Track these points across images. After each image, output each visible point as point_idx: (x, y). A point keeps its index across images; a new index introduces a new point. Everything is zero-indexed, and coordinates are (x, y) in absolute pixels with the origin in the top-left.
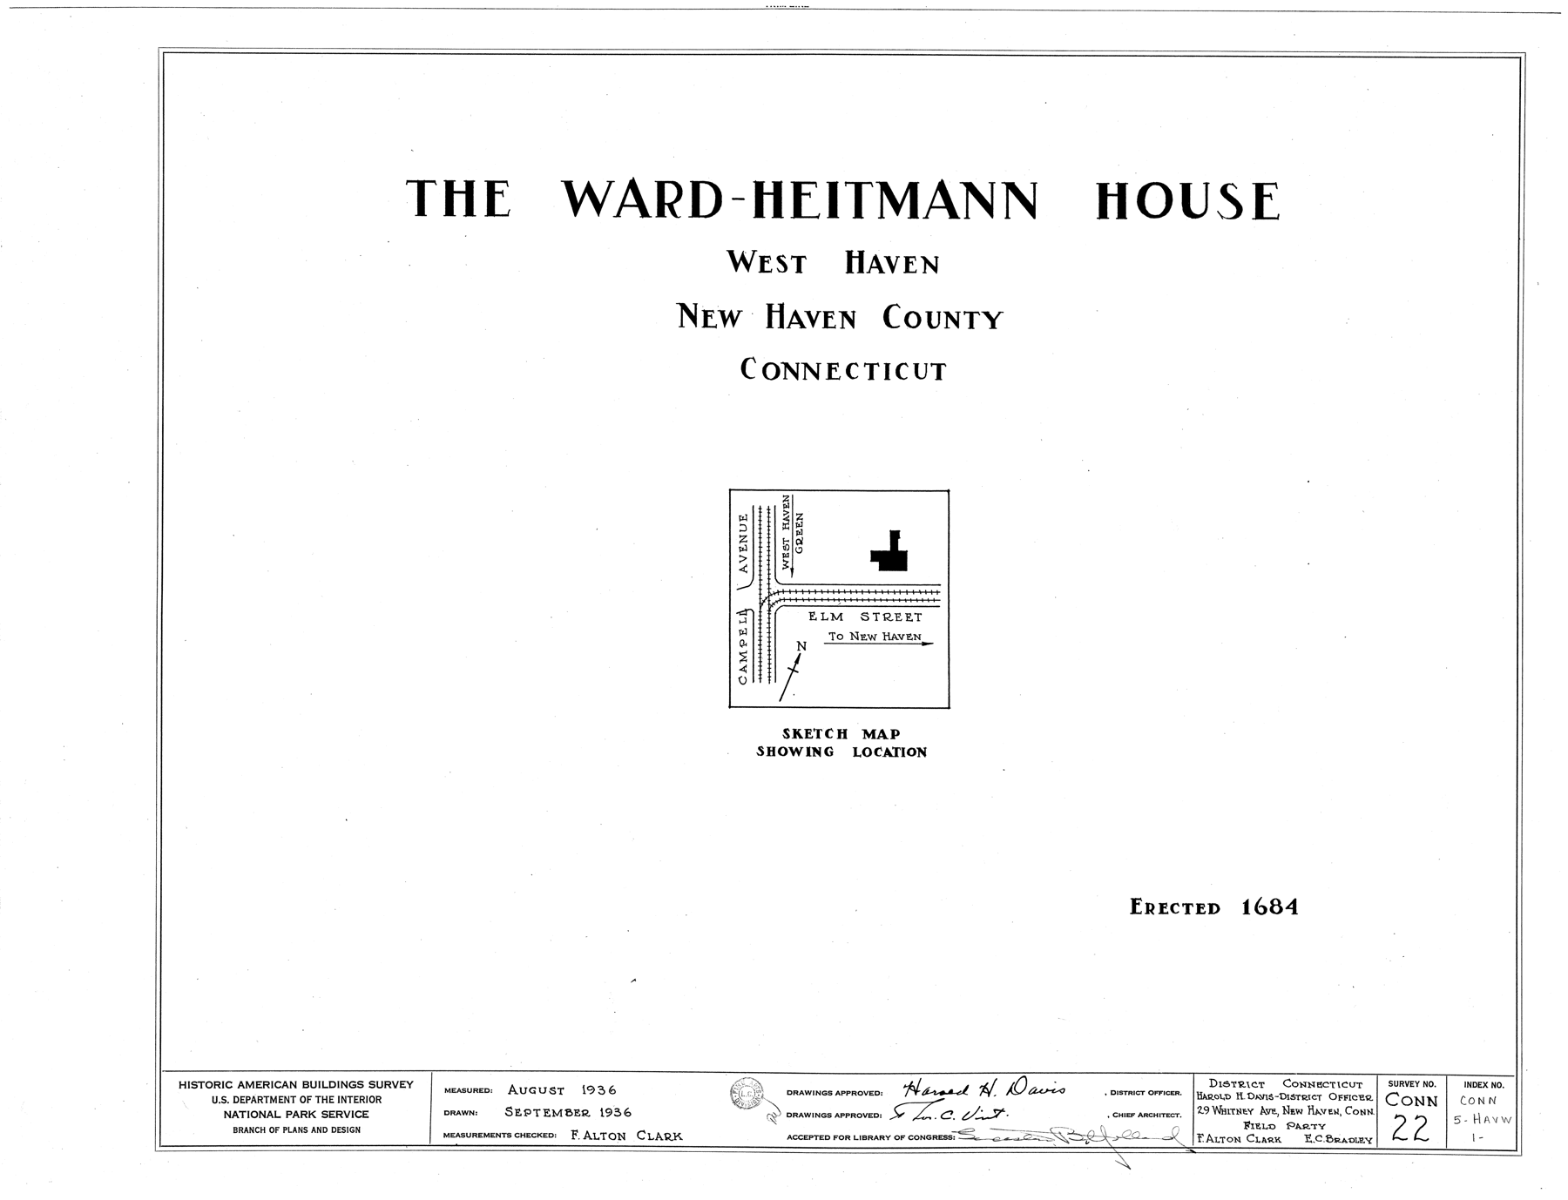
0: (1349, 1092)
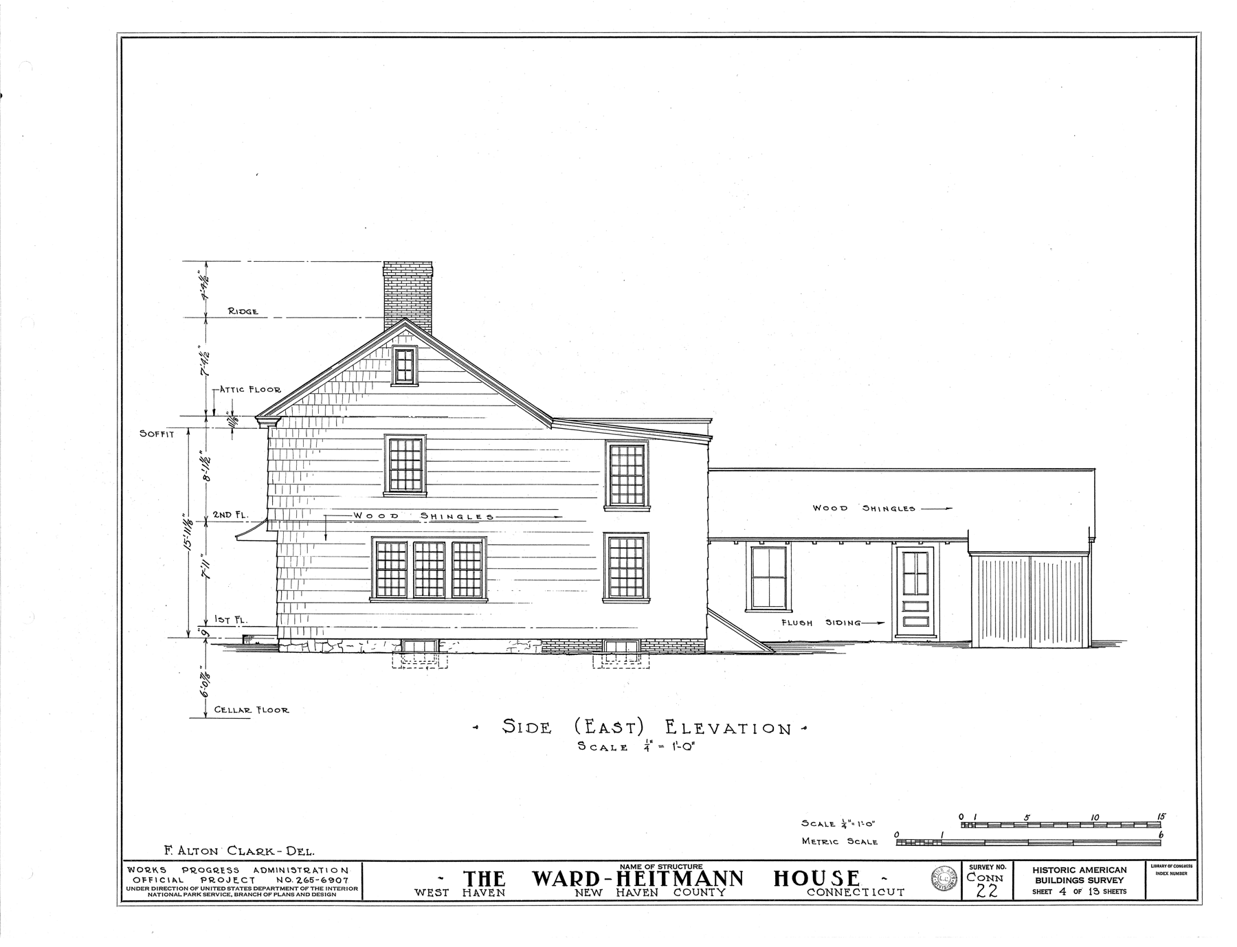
0: (923, 841)
